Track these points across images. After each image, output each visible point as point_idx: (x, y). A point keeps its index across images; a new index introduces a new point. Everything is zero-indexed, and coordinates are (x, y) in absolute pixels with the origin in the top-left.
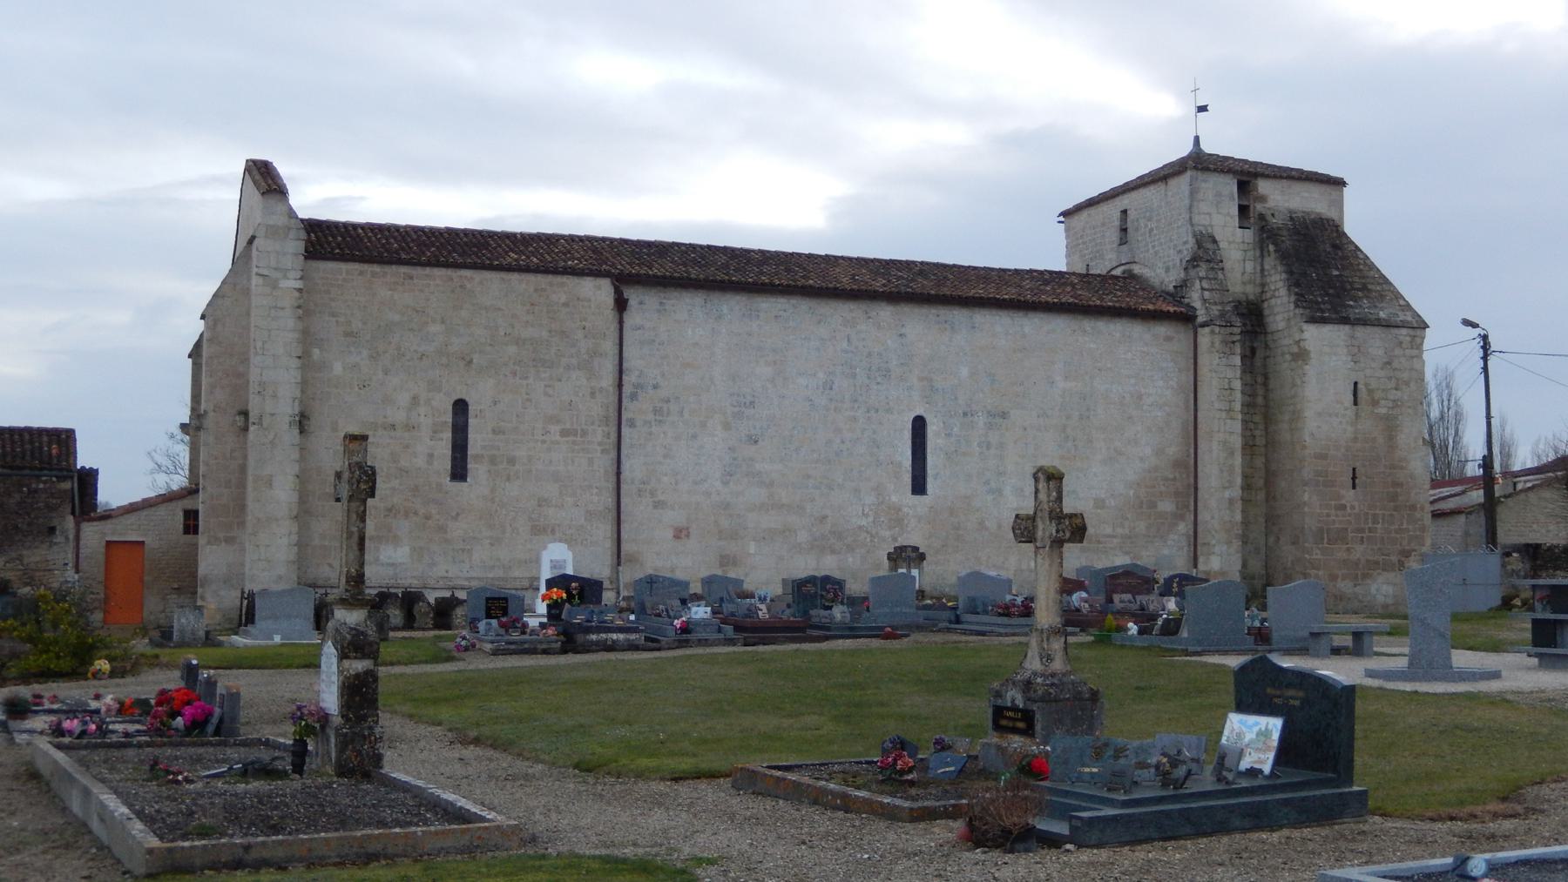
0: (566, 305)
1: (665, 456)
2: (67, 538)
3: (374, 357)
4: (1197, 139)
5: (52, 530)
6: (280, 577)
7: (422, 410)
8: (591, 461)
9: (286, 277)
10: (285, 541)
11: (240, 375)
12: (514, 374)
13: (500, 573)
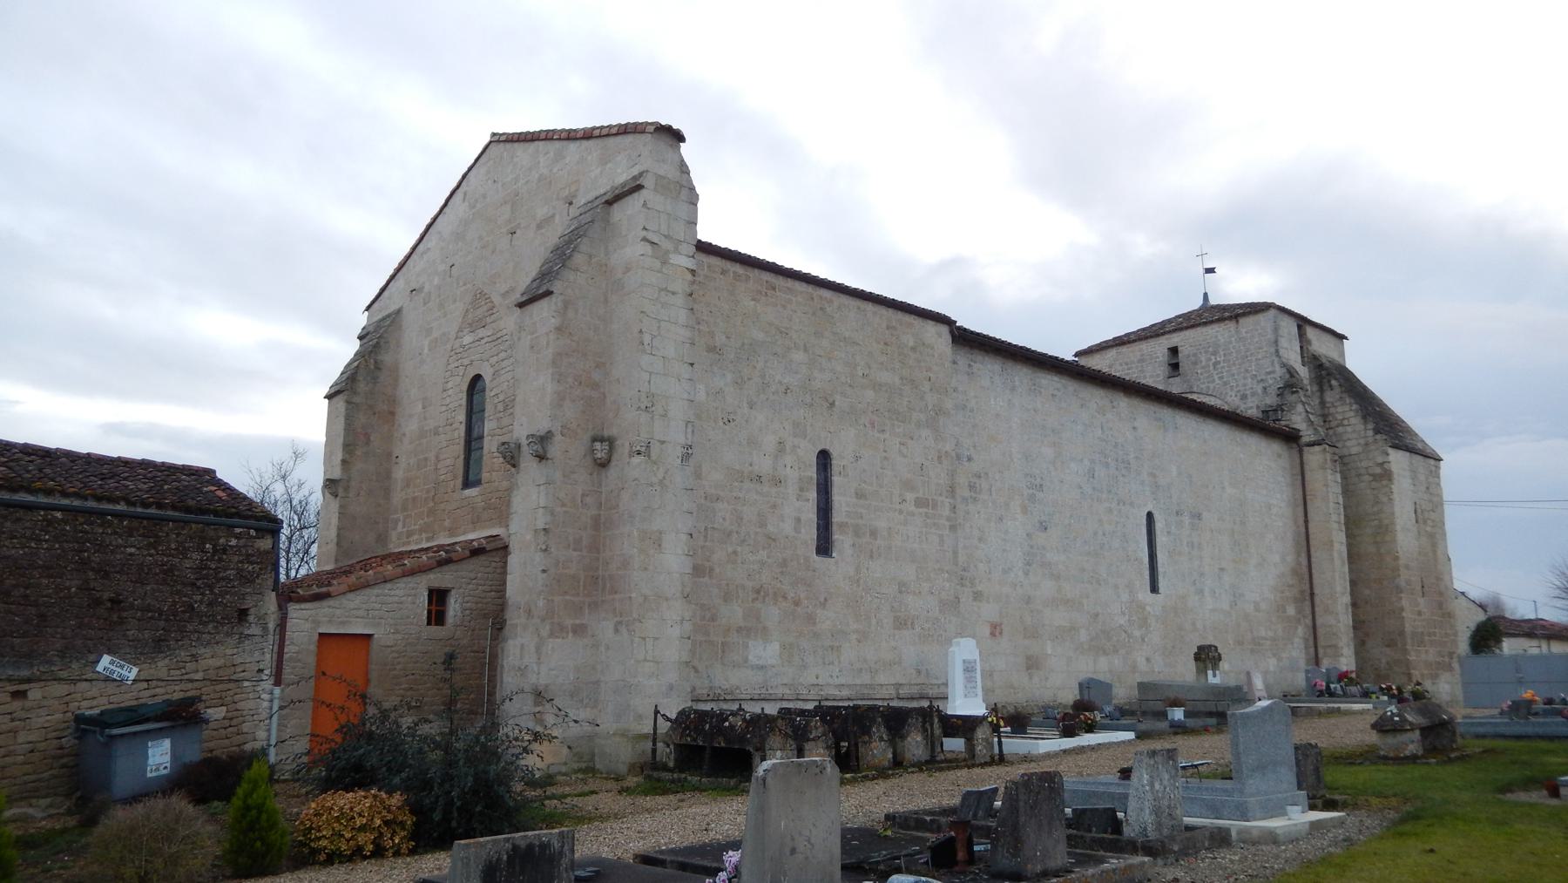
0: (913, 349)
1: (980, 539)
2: (265, 629)
3: (739, 383)
4: (1206, 295)
5: (243, 614)
6: (671, 687)
7: (788, 459)
8: (941, 536)
9: (677, 251)
10: (676, 632)
11: (595, 386)
12: (873, 425)
13: (866, 679)
